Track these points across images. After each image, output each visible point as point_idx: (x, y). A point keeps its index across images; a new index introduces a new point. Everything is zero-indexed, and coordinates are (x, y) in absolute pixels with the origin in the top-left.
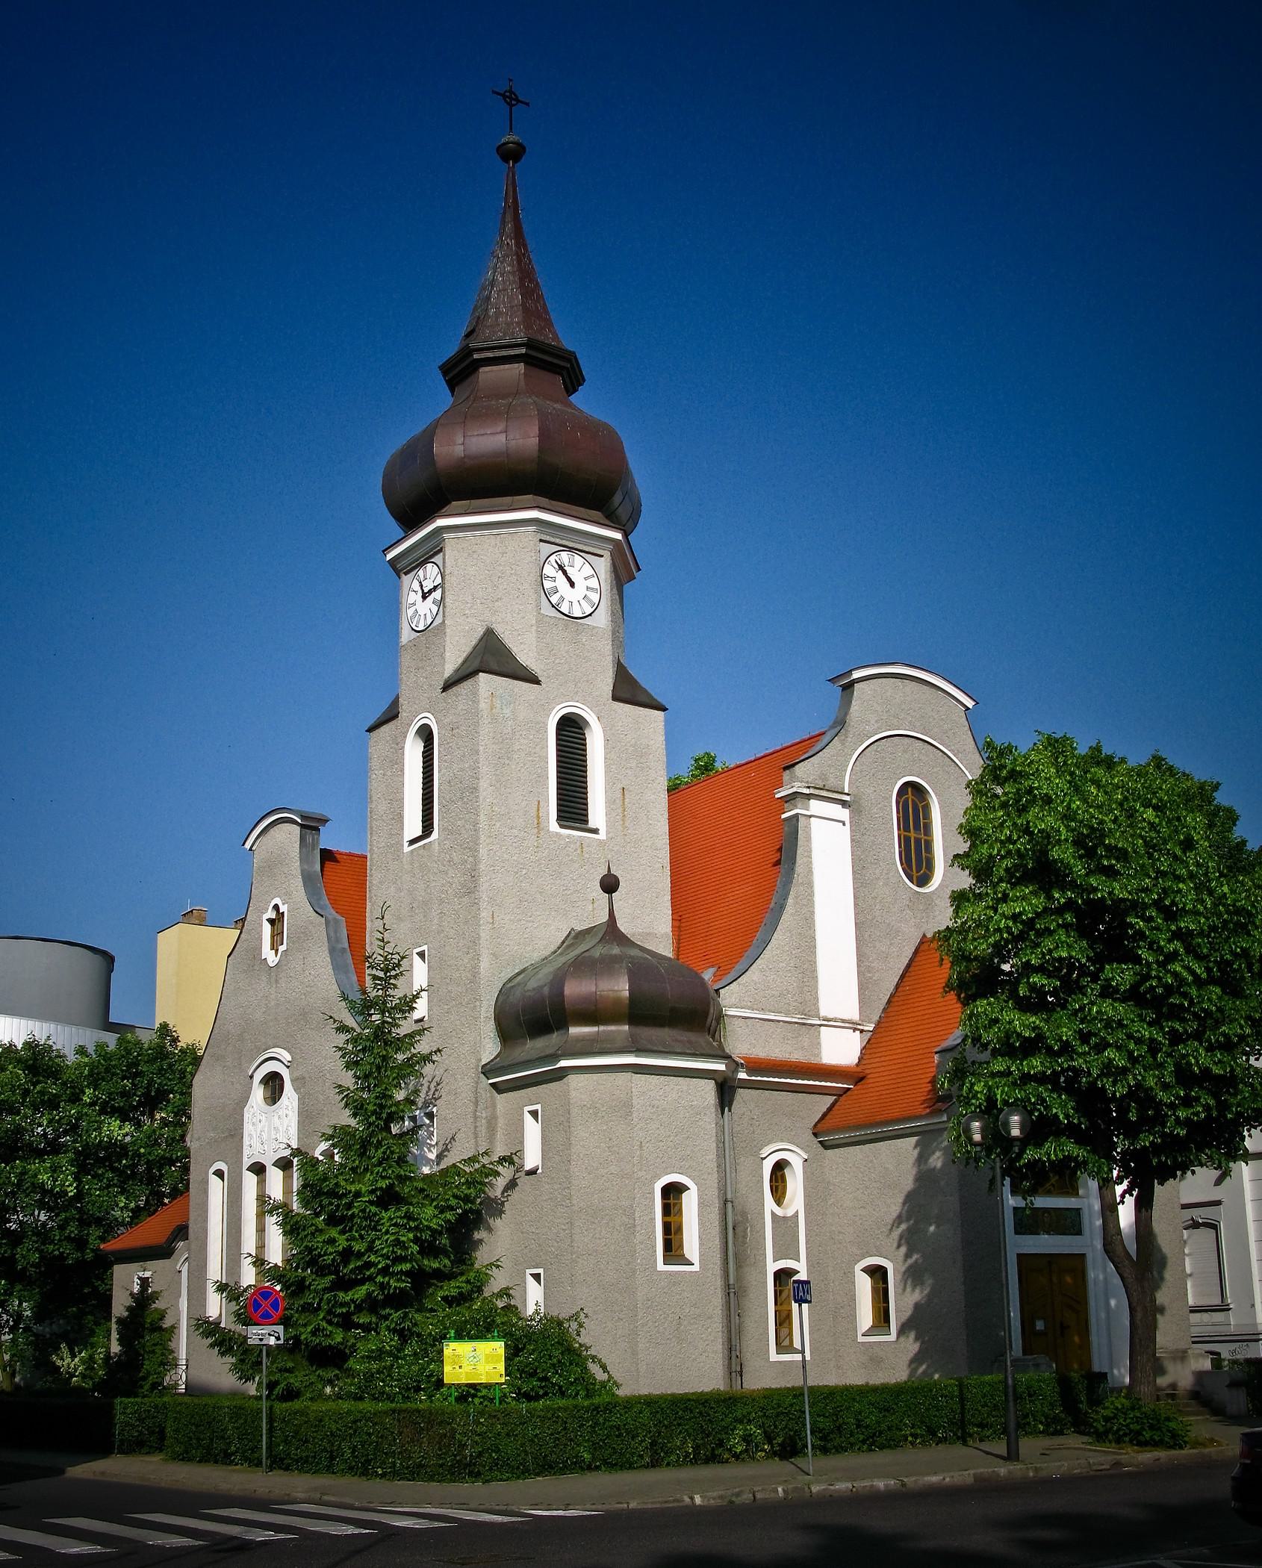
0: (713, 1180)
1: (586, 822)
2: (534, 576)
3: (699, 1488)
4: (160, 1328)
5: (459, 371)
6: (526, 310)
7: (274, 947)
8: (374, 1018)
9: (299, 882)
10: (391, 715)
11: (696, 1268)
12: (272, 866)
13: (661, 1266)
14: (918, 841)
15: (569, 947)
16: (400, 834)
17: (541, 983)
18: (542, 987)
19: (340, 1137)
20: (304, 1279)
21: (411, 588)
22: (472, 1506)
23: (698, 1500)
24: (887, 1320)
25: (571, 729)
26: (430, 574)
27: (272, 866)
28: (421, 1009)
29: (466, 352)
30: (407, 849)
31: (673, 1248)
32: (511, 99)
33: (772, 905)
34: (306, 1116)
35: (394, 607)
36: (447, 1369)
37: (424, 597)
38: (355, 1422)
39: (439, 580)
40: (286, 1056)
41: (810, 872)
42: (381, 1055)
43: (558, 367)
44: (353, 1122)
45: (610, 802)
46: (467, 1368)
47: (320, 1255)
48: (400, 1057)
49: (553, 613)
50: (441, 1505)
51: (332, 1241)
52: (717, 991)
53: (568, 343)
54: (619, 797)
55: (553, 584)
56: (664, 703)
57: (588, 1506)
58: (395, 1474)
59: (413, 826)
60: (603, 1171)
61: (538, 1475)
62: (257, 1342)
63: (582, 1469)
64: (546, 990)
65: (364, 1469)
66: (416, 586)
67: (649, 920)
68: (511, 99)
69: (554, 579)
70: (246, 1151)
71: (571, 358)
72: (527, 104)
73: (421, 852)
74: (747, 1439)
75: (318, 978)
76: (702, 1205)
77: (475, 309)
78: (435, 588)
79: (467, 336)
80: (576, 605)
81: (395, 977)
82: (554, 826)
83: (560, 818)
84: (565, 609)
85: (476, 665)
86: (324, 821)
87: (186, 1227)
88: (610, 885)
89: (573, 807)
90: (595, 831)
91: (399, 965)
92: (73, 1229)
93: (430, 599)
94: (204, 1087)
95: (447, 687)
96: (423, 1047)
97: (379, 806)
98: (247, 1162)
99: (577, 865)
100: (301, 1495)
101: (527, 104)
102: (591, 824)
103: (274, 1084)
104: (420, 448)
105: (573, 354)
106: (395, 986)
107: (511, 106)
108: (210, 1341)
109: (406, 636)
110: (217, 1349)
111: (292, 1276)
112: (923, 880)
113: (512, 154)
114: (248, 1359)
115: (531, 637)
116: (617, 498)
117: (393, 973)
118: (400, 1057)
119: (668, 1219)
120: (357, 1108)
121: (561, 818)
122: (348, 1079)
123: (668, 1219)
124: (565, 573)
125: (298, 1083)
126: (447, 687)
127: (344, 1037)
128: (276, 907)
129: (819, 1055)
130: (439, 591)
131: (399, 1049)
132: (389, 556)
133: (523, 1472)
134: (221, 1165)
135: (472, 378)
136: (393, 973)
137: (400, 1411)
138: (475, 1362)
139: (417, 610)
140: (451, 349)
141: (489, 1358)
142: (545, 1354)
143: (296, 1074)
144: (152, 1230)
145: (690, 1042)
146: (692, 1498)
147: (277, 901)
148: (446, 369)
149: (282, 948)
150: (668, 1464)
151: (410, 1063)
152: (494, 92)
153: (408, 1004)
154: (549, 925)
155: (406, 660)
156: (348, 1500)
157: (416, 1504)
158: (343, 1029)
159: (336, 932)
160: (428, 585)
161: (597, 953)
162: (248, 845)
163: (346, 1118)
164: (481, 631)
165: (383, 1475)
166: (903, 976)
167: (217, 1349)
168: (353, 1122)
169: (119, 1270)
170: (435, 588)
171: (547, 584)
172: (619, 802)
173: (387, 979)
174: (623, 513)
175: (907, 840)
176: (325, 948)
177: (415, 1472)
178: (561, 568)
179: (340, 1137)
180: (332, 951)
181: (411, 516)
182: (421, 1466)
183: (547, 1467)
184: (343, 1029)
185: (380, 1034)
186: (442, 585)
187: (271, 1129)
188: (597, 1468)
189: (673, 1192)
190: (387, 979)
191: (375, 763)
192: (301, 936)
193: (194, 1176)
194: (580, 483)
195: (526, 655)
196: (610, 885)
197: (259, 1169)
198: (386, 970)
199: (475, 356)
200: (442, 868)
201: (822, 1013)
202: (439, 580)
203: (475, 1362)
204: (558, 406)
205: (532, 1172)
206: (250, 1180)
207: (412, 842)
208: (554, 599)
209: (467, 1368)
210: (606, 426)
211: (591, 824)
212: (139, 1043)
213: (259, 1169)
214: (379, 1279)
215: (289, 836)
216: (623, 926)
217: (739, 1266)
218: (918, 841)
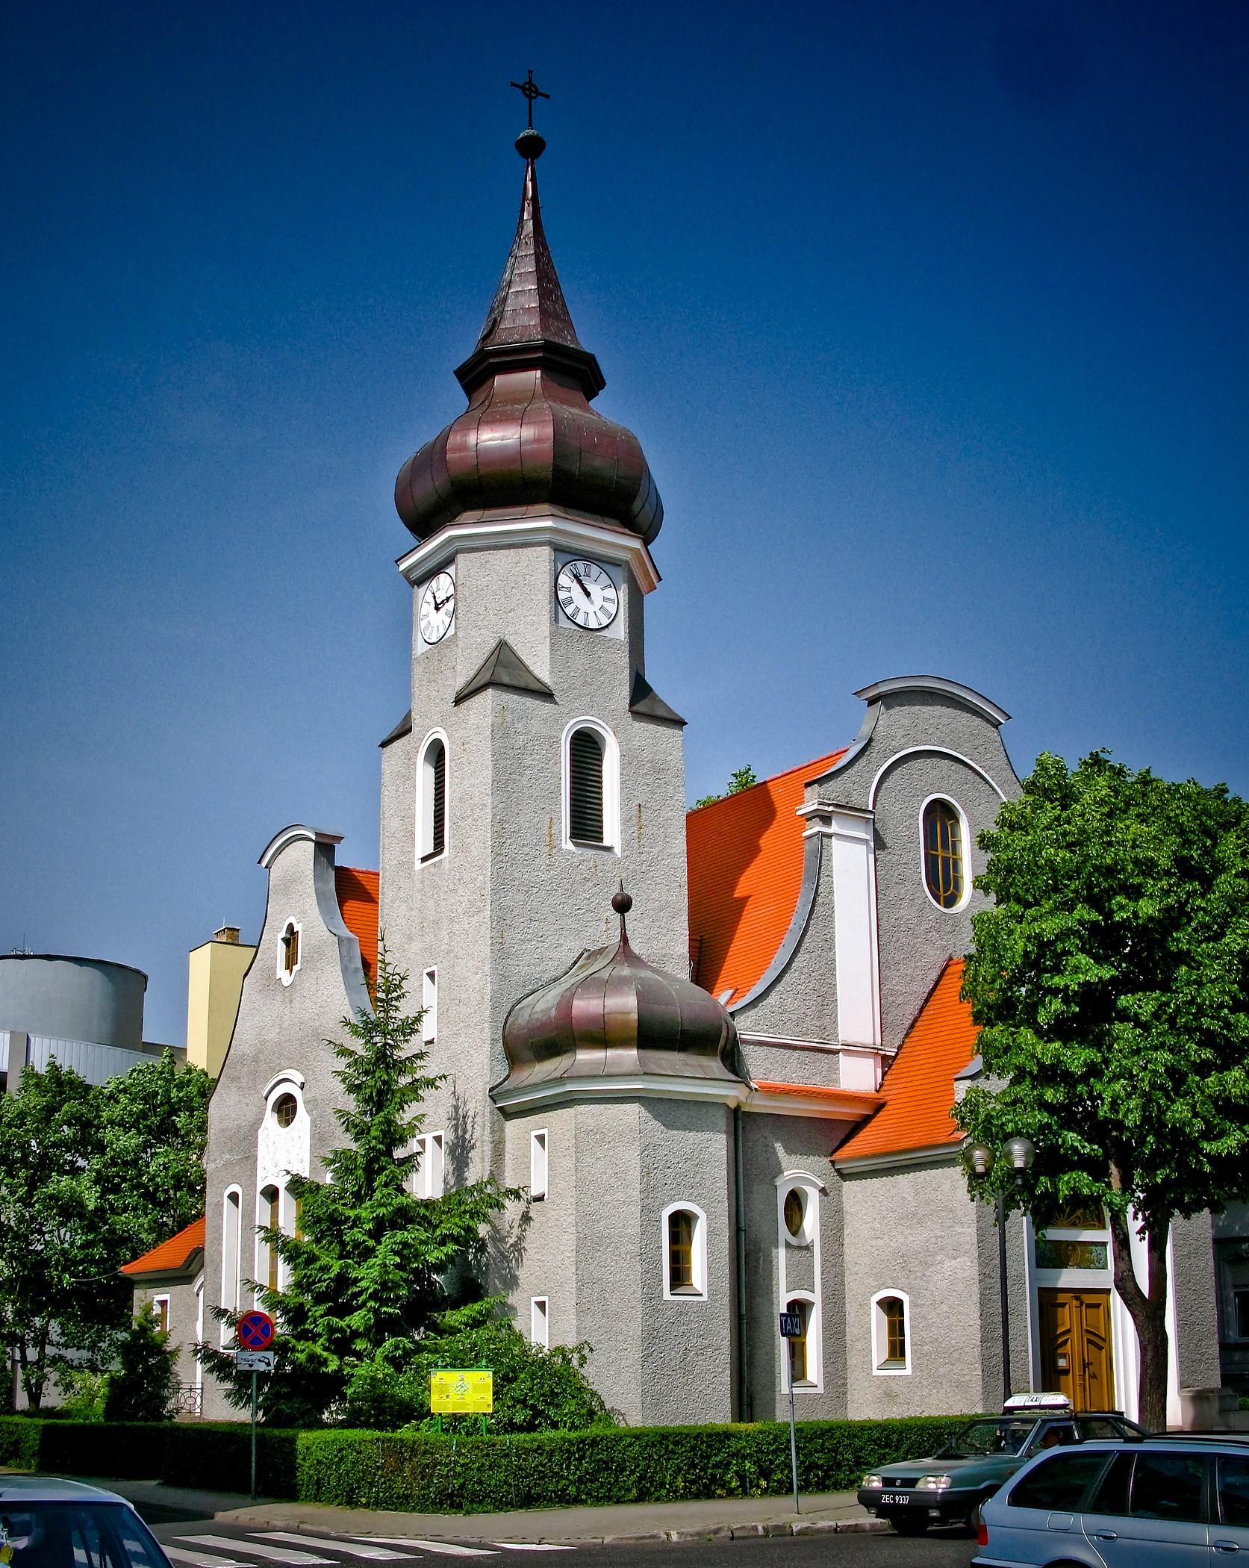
0: (723, 1208)
1: (601, 840)
2: (546, 588)
3: (675, 1521)
4: (165, 1352)
5: (475, 376)
6: (543, 310)
7: (289, 966)
8: (377, 1039)
9: (312, 900)
10: (404, 730)
11: (705, 1298)
12: (289, 882)
13: (667, 1295)
14: (946, 860)
15: (581, 967)
16: (412, 852)
17: (547, 1005)
18: (550, 1009)
19: (342, 1163)
20: (302, 1305)
21: (424, 596)
22: (447, 1538)
23: (675, 1538)
24: (903, 1354)
25: (586, 748)
26: (442, 585)
27: (290, 882)
28: (428, 1029)
29: (481, 355)
30: (419, 866)
31: (679, 1276)
32: (531, 91)
33: (791, 926)
34: (318, 1137)
35: (405, 622)
36: (434, 1398)
37: (437, 608)
38: (341, 1450)
39: (451, 591)
40: (299, 1078)
41: (831, 893)
42: (382, 1079)
43: (575, 372)
44: (354, 1146)
45: (625, 821)
46: (454, 1398)
47: (314, 1283)
48: (404, 1081)
49: (569, 625)
50: (417, 1536)
51: (324, 1269)
52: (732, 1014)
53: (586, 343)
54: (636, 815)
55: (567, 595)
56: (681, 712)
57: (563, 1540)
58: (377, 1504)
59: (424, 843)
60: (609, 1198)
61: (521, 1507)
62: (247, 1368)
63: (568, 1502)
64: (553, 1013)
65: (350, 1500)
66: (429, 597)
67: (665, 939)
68: (530, 91)
69: (569, 589)
70: (260, 1173)
71: (590, 360)
72: (548, 97)
73: (432, 870)
74: (741, 1476)
75: (330, 997)
76: (711, 1233)
77: (492, 310)
78: (448, 599)
79: (485, 338)
80: (592, 617)
81: (398, 998)
82: (568, 845)
83: (573, 836)
84: (580, 620)
85: (485, 677)
86: (339, 839)
87: (203, 1249)
88: (622, 905)
89: (586, 824)
90: (609, 849)
91: (400, 986)
92: (99, 1252)
93: (443, 610)
94: (222, 1111)
95: (459, 700)
96: (429, 1069)
97: (390, 824)
98: (260, 1186)
99: (590, 884)
100: (279, 1523)
101: (548, 97)
102: (606, 843)
103: (286, 1108)
104: (433, 456)
105: (592, 357)
106: (397, 1009)
107: (530, 98)
108: (209, 1365)
109: (420, 648)
110: (215, 1374)
111: (292, 1303)
112: (950, 901)
113: (530, 148)
114: (243, 1384)
115: (545, 649)
116: (637, 505)
117: (395, 994)
118: (404, 1081)
119: (676, 1248)
120: (361, 1132)
121: (574, 835)
122: (351, 1104)
123: (676, 1248)
124: (580, 582)
125: (312, 1105)
126: (459, 700)
127: (345, 1060)
128: (291, 927)
129: (837, 1081)
130: (452, 602)
131: (401, 1072)
132: (402, 567)
133: (503, 1504)
134: (235, 1188)
135: (489, 383)
136: (395, 994)
137: (390, 1440)
138: (462, 1391)
139: (431, 622)
140: (465, 353)
141: (476, 1388)
142: (540, 1388)
143: (309, 1096)
144: (168, 1254)
145: (701, 1066)
146: (668, 1535)
147: (292, 920)
148: (462, 373)
149: (296, 968)
150: (658, 1499)
151: (414, 1086)
152: (513, 84)
153: (410, 1027)
154: (561, 945)
155: (418, 672)
156: (325, 1529)
157: (392, 1536)
158: (343, 1052)
159: (349, 950)
160: (441, 596)
161: (605, 975)
162: (264, 864)
163: (346, 1142)
164: (493, 644)
165: (367, 1506)
166: (927, 1000)
167: (215, 1374)
168: (354, 1146)
169: (138, 1294)
170: (448, 599)
171: (562, 595)
172: (635, 821)
173: (387, 1001)
174: (643, 519)
175: (954, 852)
176: (338, 968)
177: (400, 1502)
178: (577, 578)
179: (342, 1163)
180: (345, 970)
181: (423, 525)
182: (406, 1497)
183: (528, 1501)
184: (343, 1052)
185: (383, 1059)
186: (454, 596)
187: (286, 1152)
188: (583, 1502)
189: (681, 1223)
190: (387, 1001)
191: (386, 779)
192: (317, 953)
193: (210, 1198)
194: (599, 490)
195: (541, 667)
196: (622, 905)
197: (271, 1194)
198: (388, 992)
199: (492, 361)
200: (452, 887)
201: (840, 1038)
202: (451, 591)
203: (462, 1391)
204: (575, 411)
205: (540, 1199)
206: (262, 1206)
207: (424, 859)
208: (569, 610)
209: (454, 1398)
210: (626, 432)
211: (606, 843)
212: (1151, 919)
213: (271, 1194)
214: (371, 1304)
215: (304, 853)
216: (635, 947)
217: (751, 1298)
218: (946, 860)
